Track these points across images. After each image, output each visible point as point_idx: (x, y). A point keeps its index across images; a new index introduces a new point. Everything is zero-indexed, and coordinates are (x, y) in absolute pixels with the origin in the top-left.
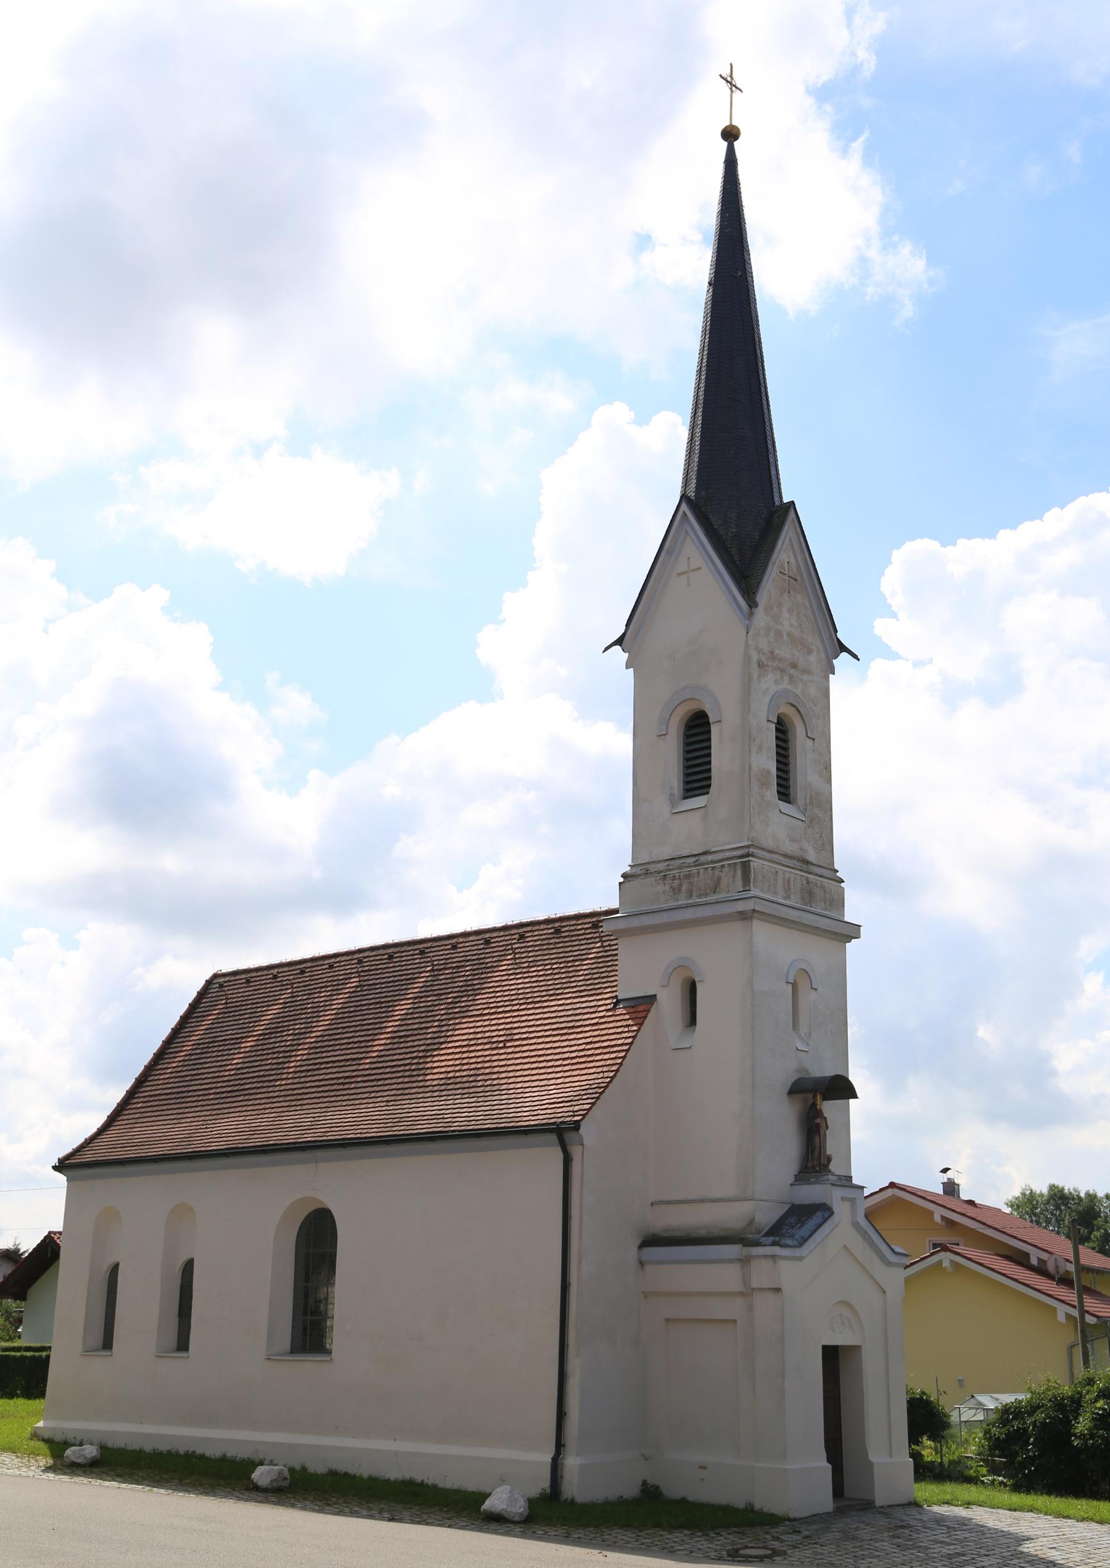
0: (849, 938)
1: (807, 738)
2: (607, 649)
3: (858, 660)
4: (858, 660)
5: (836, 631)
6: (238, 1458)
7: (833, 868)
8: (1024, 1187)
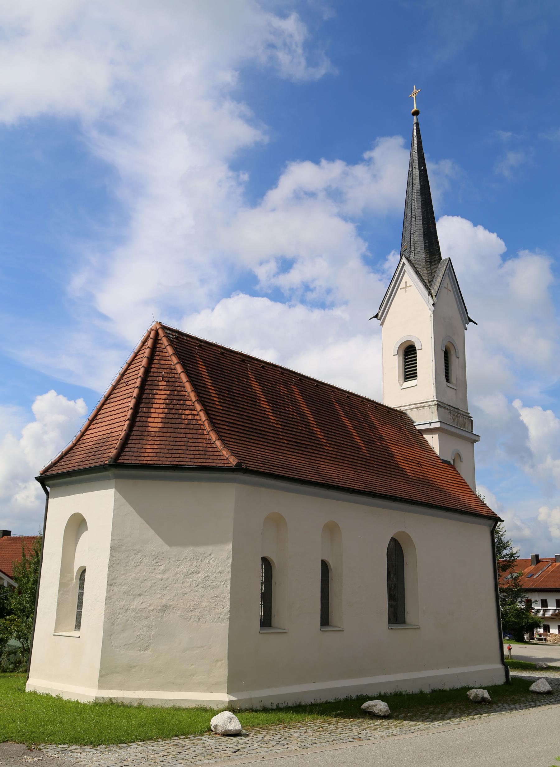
0: (475, 441)
1: (447, 387)
2: (370, 319)
3: (477, 325)
4: (477, 325)
5: (467, 313)
6: (375, 695)
7: (467, 412)
8: (337, 698)
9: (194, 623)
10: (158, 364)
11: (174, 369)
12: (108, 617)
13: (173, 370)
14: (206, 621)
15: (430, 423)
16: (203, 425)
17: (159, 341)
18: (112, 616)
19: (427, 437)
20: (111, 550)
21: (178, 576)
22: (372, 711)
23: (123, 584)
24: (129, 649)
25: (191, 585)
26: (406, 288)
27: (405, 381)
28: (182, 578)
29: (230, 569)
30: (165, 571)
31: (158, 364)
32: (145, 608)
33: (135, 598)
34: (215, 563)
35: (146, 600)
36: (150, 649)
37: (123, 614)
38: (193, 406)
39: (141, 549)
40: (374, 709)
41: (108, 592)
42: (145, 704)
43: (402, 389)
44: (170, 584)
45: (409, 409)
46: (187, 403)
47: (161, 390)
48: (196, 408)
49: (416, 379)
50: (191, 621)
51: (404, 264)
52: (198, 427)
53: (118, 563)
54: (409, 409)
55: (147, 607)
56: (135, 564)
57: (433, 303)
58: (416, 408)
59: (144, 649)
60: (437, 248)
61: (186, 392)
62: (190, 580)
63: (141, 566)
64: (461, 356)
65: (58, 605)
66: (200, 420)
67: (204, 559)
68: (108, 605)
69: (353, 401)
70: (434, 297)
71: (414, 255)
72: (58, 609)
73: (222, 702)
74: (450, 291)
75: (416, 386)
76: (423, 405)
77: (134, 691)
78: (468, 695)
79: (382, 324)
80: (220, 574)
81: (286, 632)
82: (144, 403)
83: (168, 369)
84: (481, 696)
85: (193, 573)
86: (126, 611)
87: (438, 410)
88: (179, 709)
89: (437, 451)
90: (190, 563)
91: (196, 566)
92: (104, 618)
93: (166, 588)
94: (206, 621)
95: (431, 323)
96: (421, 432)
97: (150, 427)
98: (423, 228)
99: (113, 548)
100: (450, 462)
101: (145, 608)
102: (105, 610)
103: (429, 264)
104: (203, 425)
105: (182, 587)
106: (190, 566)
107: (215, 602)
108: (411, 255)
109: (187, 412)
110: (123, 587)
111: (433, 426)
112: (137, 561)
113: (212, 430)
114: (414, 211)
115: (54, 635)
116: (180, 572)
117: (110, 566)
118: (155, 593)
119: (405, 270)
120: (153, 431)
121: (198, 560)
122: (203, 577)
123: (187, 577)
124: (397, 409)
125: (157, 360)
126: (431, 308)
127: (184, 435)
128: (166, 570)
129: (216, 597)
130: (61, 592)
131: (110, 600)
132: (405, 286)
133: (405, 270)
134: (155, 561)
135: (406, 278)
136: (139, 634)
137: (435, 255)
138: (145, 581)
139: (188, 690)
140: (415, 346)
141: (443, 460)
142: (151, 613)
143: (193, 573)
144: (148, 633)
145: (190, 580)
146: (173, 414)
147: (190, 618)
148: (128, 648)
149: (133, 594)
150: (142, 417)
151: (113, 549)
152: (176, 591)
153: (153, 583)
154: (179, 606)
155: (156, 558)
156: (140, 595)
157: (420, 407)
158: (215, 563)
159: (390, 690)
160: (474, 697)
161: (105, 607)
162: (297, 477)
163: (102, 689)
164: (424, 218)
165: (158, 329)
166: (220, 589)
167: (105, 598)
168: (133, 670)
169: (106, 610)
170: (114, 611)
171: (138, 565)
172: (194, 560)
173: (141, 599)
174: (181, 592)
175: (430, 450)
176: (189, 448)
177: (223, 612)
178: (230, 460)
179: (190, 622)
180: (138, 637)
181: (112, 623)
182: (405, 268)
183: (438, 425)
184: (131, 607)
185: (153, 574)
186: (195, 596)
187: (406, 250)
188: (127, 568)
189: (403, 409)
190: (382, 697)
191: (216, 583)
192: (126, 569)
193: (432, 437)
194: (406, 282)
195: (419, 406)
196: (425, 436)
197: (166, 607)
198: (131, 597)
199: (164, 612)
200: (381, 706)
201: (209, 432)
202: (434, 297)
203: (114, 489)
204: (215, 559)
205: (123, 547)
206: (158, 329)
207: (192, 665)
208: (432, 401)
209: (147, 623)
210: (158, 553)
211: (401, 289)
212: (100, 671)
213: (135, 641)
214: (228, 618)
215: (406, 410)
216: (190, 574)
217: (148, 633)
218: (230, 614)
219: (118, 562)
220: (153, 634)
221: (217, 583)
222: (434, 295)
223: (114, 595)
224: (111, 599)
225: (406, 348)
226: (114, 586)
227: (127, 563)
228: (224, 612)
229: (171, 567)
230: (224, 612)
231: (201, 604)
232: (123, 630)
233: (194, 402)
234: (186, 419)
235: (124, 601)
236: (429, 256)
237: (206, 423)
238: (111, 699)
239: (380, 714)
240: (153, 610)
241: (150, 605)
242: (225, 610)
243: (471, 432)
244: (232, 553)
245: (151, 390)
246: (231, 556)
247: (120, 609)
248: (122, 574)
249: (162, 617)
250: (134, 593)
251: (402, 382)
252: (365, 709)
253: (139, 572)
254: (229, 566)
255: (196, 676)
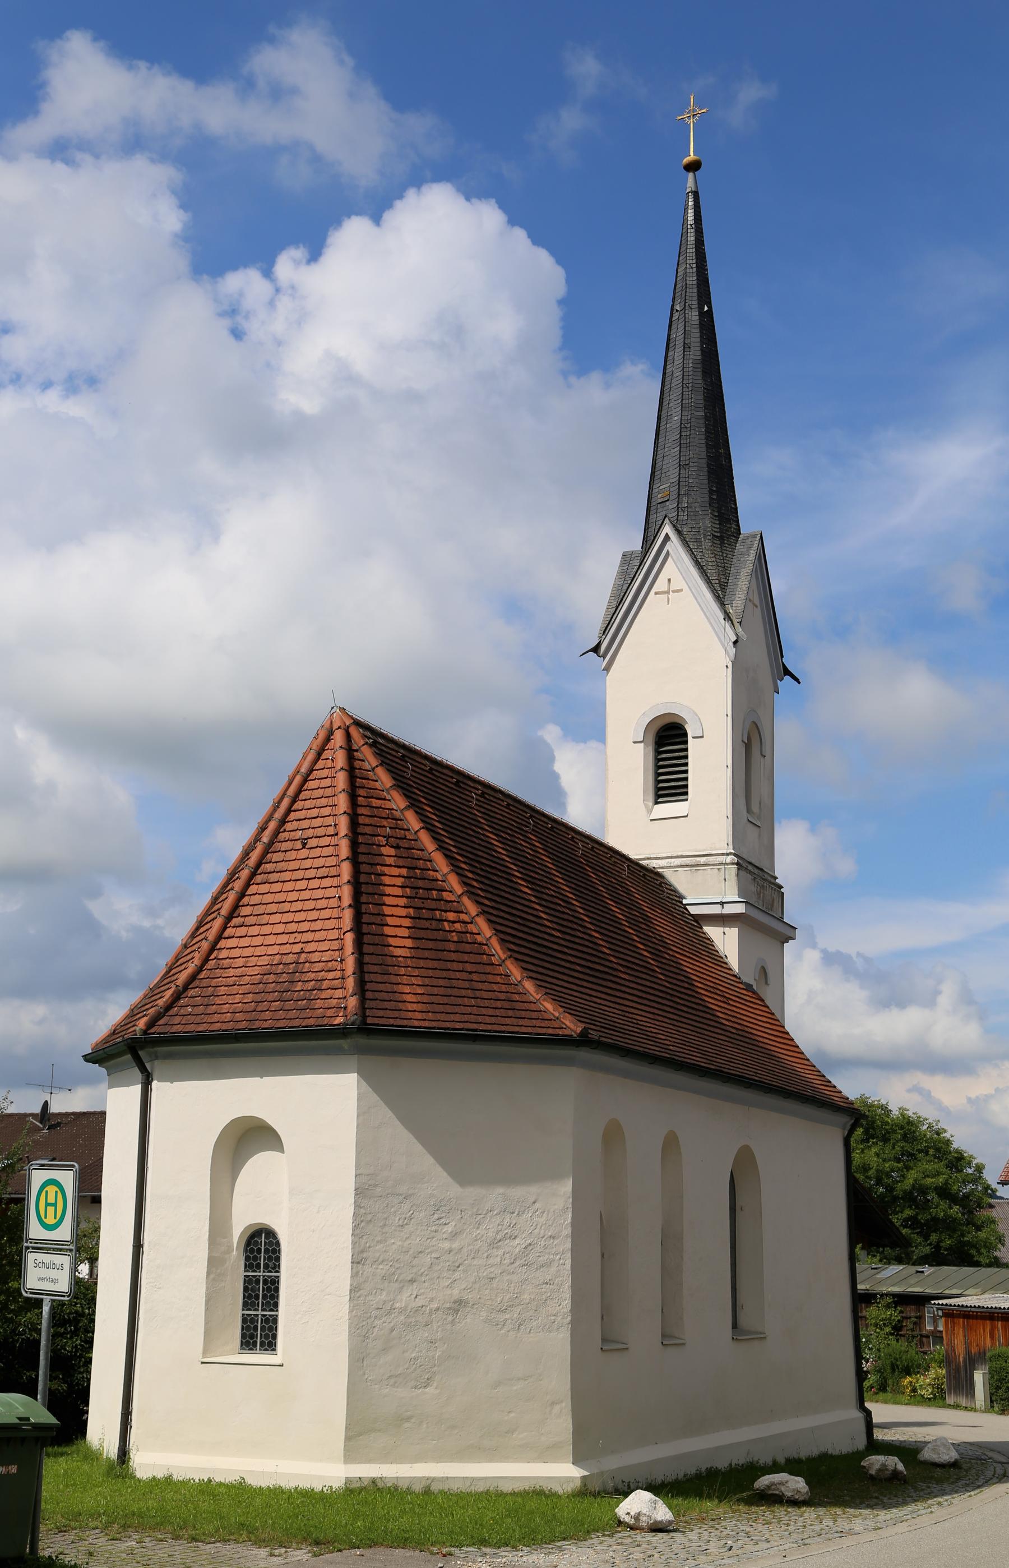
0: (787, 939)
3: (799, 683)
4: (799, 683)
5: (782, 656)
9: (510, 1333)
10: (367, 806)
11: (401, 820)
12: (357, 1325)
13: (399, 822)
14: (531, 1330)
15: (722, 903)
16: (486, 945)
17: (355, 753)
18: (364, 1323)
19: (712, 932)
20: (356, 1195)
21: (479, 1244)
22: (777, 1492)
23: (380, 1260)
24: (396, 1385)
25: (503, 1262)
26: (668, 592)
27: (656, 803)
28: (486, 1249)
29: (569, 1230)
30: (454, 1235)
31: (367, 806)
32: (422, 1307)
33: (403, 1286)
34: (542, 1220)
35: (423, 1291)
36: (435, 1385)
37: (384, 1319)
38: (458, 902)
39: (410, 1192)
40: (783, 1489)
41: (354, 1275)
42: (435, 1488)
43: (651, 820)
44: (465, 1260)
45: (670, 867)
46: (445, 895)
47: (390, 866)
48: (466, 908)
49: (686, 800)
50: (506, 1329)
51: (667, 538)
52: (480, 949)
53: (370, 1221)
54: (670, 867)
55: (427, 1304)
56: (401, 1223)
57: (734, 638)
58: (687, 866)
59: (423, 1385)
60: (733, 506)
61: (437, 871)
62: (500, 1252)
63: (411, 1225)
64: (767, 751)
65: (207, 1302)
66: (479, 934)
67: (524, 1212)
68: (355, 1302)
69: (601, 857)
70: (737, 625)
71: (685, 518)
72: (207, 1309)
73: (569, 1479)
74: (756, 606)
75: (687, 816)
76: (703, 860)
77: (410, 1465)
78: (864, 1467)
79: (607, 669)
80: (552, 1241)
81: (627, 1349)
82: (366, 894)
83: (388, 818)
84: (891, 1468)
85: (504, 1238)
86: (389, 1312)
87: (738, 875)
88: (501, 1494)
89: (734, 962)
90: (498, 1219)
91: (510, 1226)
92: (350, 1327)
93: (458, 1267)
94: (531, 1330)
95: (727, 676)
96: (700, 920)
97: (391, 946)
98: (707, 456)
99: (360, 1190)
100: (752, 985)
101: (422, 1307)
102: (351, 1311)
103: (719, 542)
104: (486, 945)
105: (485, 1266)
106: (499, 1225)
107: (545, 1292)
108: (680, 518)
109: (451, 916)
110: (381, 1267)
111: (729, 909)
112: (404, 1216)
113: (509, 958)
114: (686, 413)
115: (203, 1363)
116: (483, 1235)
117: (355, 1226)
118: (439, 1277)
119: (668, 551)
120: (400, 956)
121: (513, 1213)
122: (523, 1246)
123: (495, 1246)
124: (644, 863)
125: (364, 797)
126: (728, 649)
127: (460, 966)
128: (456, 1234)
129: (547, 1283)
130: (212, 1276)
131: (357, 1292)
132: (666, 589)
133: (668, 551)
134: (436, 1216)
135: (670, 570)
136: (413, 1355)
137: (728, 520)
138: (420, 1255)
139: (505, 1458)
140: (686, 727)
141: (746, 984)
142: (434, 1316)
143: (504, 1238)
144: (430, 1354)
145: (500, 1252)
146: (427, 919)
147: (502, 1323)
148: (395, 1383)
149: (400, 1279)
150: (371, 924)
151: (360, 1194)
152: (476, 1274)
153: (435, 1258)
154: (482, 1301)
155: (437, 1210)
156: (412, 1281)
157: (697, 865)
158: (542, 1220)
159: (809, 1450)
160: (879, 1470)
161: (350, 1306)
162: (668, 1056)
163: (350, 1463)
164: (709, 433)
165: (348, 727)
166: (553, 1269)
167: (348, 1288)
168: (407, 1425)
169: (353, 1311)
170: (367, 1313)
171: (407, 1224)
172: (506, 1214)
173: (414, 1289)
174: (485, 1274)
175: (720, 962)
176: (478, 994)
177: (560, 1312)
178: (564, 1021)
179: (503, 1332)
180: (412, 1363)
181: (364, 1336)
182: (668, 547)
183: (740, 909)
184: (397, 1305)
185: (434, 1242)
186: (510, 1282)
187: (667, 503)
188: (386, 1229)
189: (653, 864)
190: (793, 1466)
191: (546, 1258)
192: (384, 1231)
193: (724, 933)
194: (669, 580)
195: (695, 863)
196: (707, 929)
197: (459, 1304)
198: (397, 1285)
199: (457, 1314)
200: (796, 1484)
201: (504, 961)
202: (737, 625)
203: (356, 1074)
204: (543, 1212)
205: (378, 1189)
206: (348, 727)
207: (509, 1412)
208: (723, 854)
209: (426, 1335)
210: (440, 1201)
211: (656, 593)
212: (346, 1428)
213: (407, 1369)
214: (569, 1324)
215: (662, 868)
216: (500, 1241)
217: (430, 1354)
218: (572, 1316)
219: (369, 1217)
220: (439, 1356)
221: (547, 1256)
222: (735, 621)
223: (365, 1281)
224: (360, 1289)
225: (661, 728)
226: (363, 1264)
227: (386, 1219)
228: (562, 1311)
229: (465, 1227)
230: (562, 1311)
231: (522, 1297)
232: (385, 1350)
233: (460, 895)
234: (454, 931)
235: (384, 1293)
236: (719, 524)
237: (495, 942)
238: (374, 1481)
239: (797, 1497)
240: (438, 1309)
241: (432, 1300)
242: (563, 1308)
243: (781, 920)
244: (571, 1200)
245: (372, 864)
246: (571, 1206)
247: (378, 1309)
248: (378, 1242)
249: (453, 1322)
250: (400, 1279)
251: (650, 804)
252: (763, 1490)
253: (407, 1238)
254: (567, 1224)
255: (517, 1433)
